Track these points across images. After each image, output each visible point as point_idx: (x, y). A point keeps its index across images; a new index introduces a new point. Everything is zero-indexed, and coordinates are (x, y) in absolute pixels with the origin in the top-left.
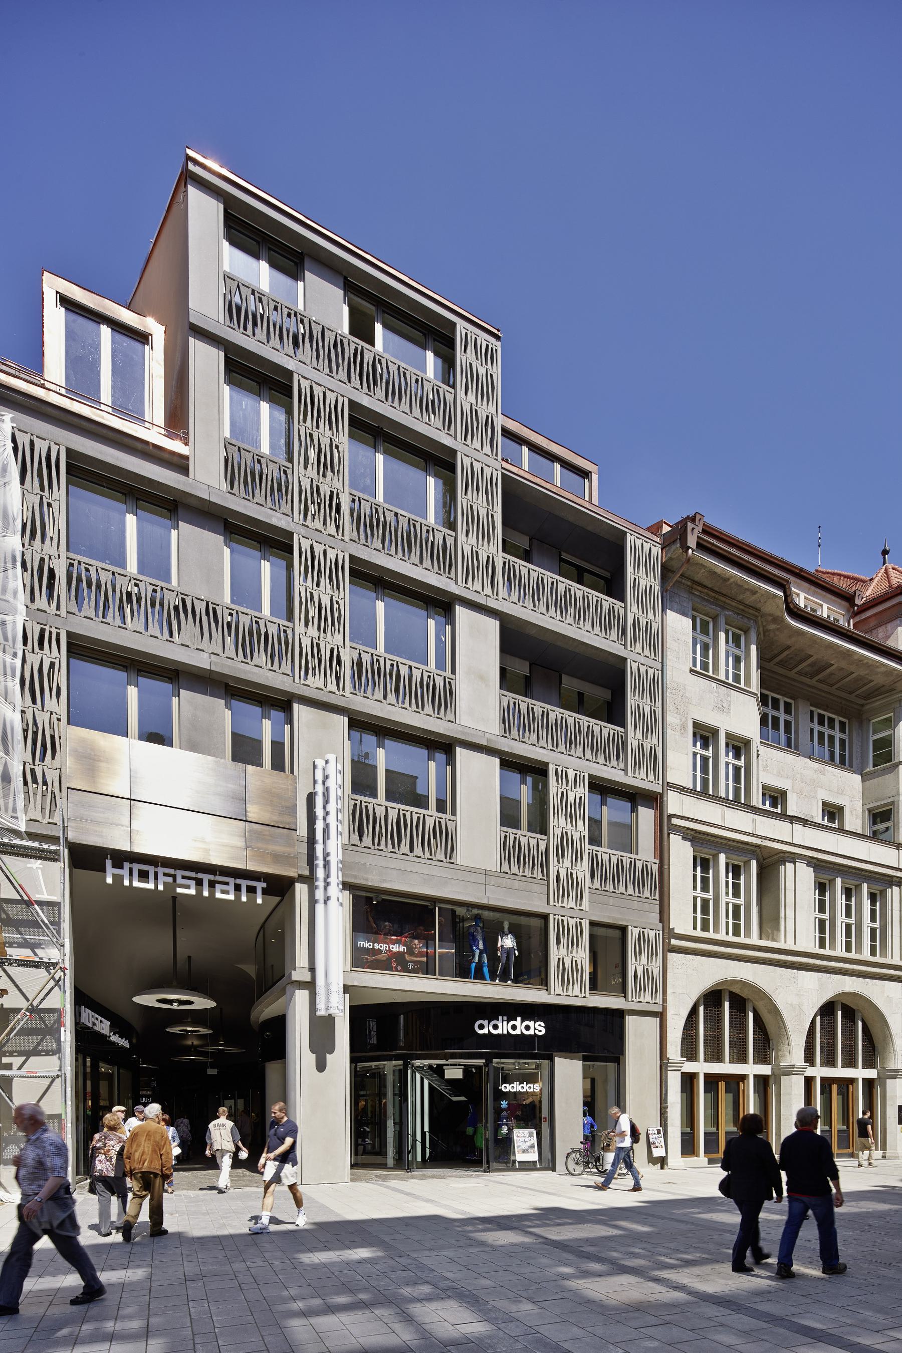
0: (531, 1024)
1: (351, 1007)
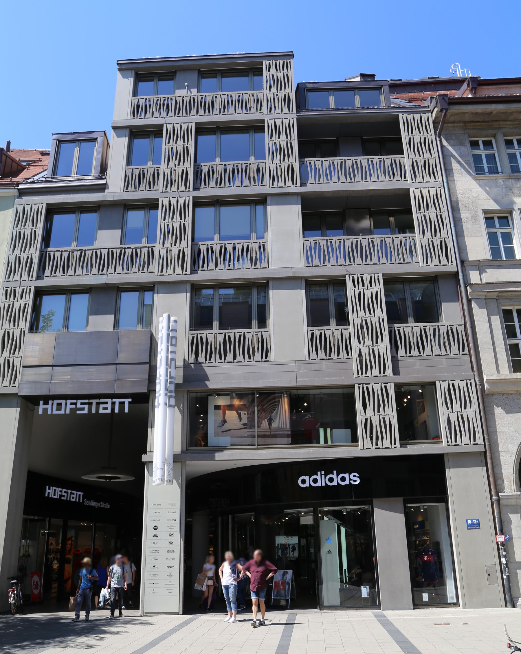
0: (346, 476)
1: (149, 403)
